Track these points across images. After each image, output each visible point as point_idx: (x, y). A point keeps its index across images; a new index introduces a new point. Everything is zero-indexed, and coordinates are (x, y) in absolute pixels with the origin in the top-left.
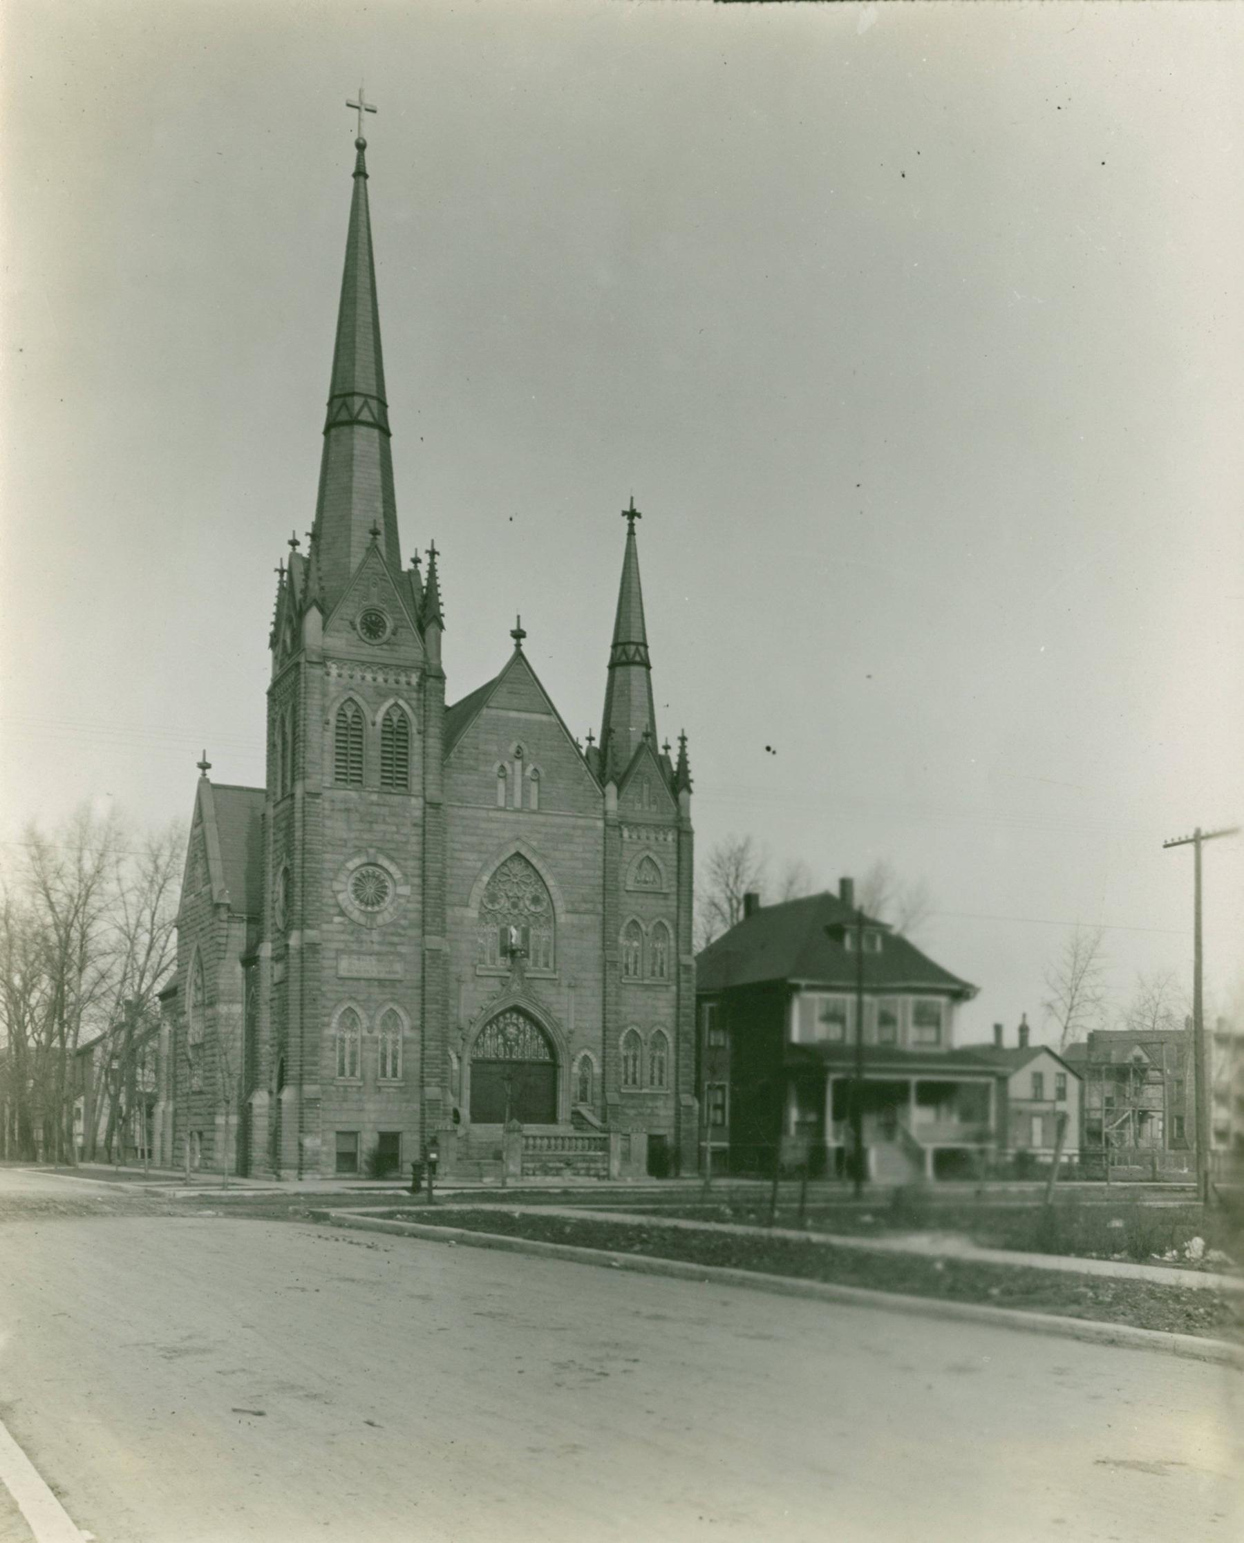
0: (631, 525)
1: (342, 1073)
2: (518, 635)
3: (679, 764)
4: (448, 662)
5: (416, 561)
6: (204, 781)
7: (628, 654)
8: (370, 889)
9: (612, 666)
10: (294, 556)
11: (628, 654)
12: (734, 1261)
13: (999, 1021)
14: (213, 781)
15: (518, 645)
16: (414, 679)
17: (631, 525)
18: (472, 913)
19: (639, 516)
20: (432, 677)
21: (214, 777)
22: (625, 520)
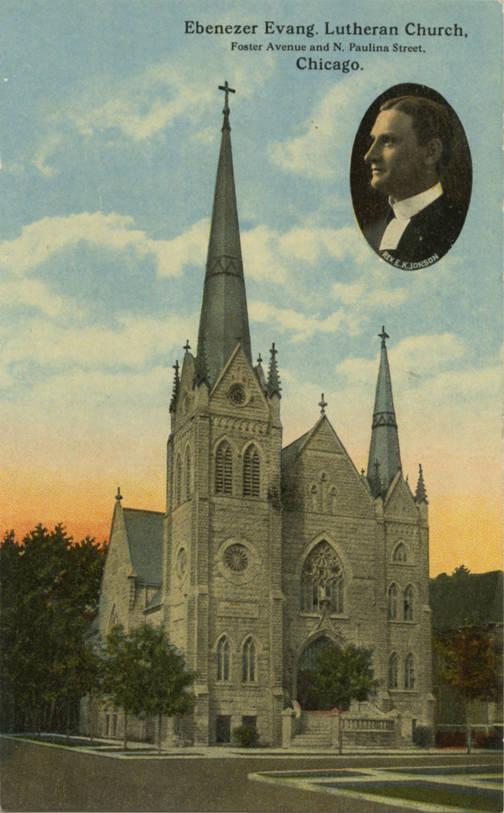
0: (383, 343)
1: (219, 678)
2: (323, 405)
3: (417, 492)
4: (285, 419)
5: (260, 360)
6: (118, 505)
7: (385, 422)
8: (236, 559)
9: (374, 427)
10: (188, 355)
11: (385, 422)
12: (344, 457)
13: (420, 462)
14: (394, 247)
15: (323, 411)
16: (264, 429)
17: (383, 343)
18: (297, 577)
19: (388, 336)
20: (273, 427)
21: (125, 504)
22: (380, 339)
